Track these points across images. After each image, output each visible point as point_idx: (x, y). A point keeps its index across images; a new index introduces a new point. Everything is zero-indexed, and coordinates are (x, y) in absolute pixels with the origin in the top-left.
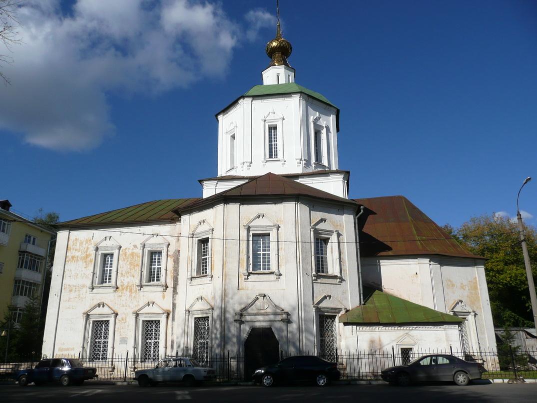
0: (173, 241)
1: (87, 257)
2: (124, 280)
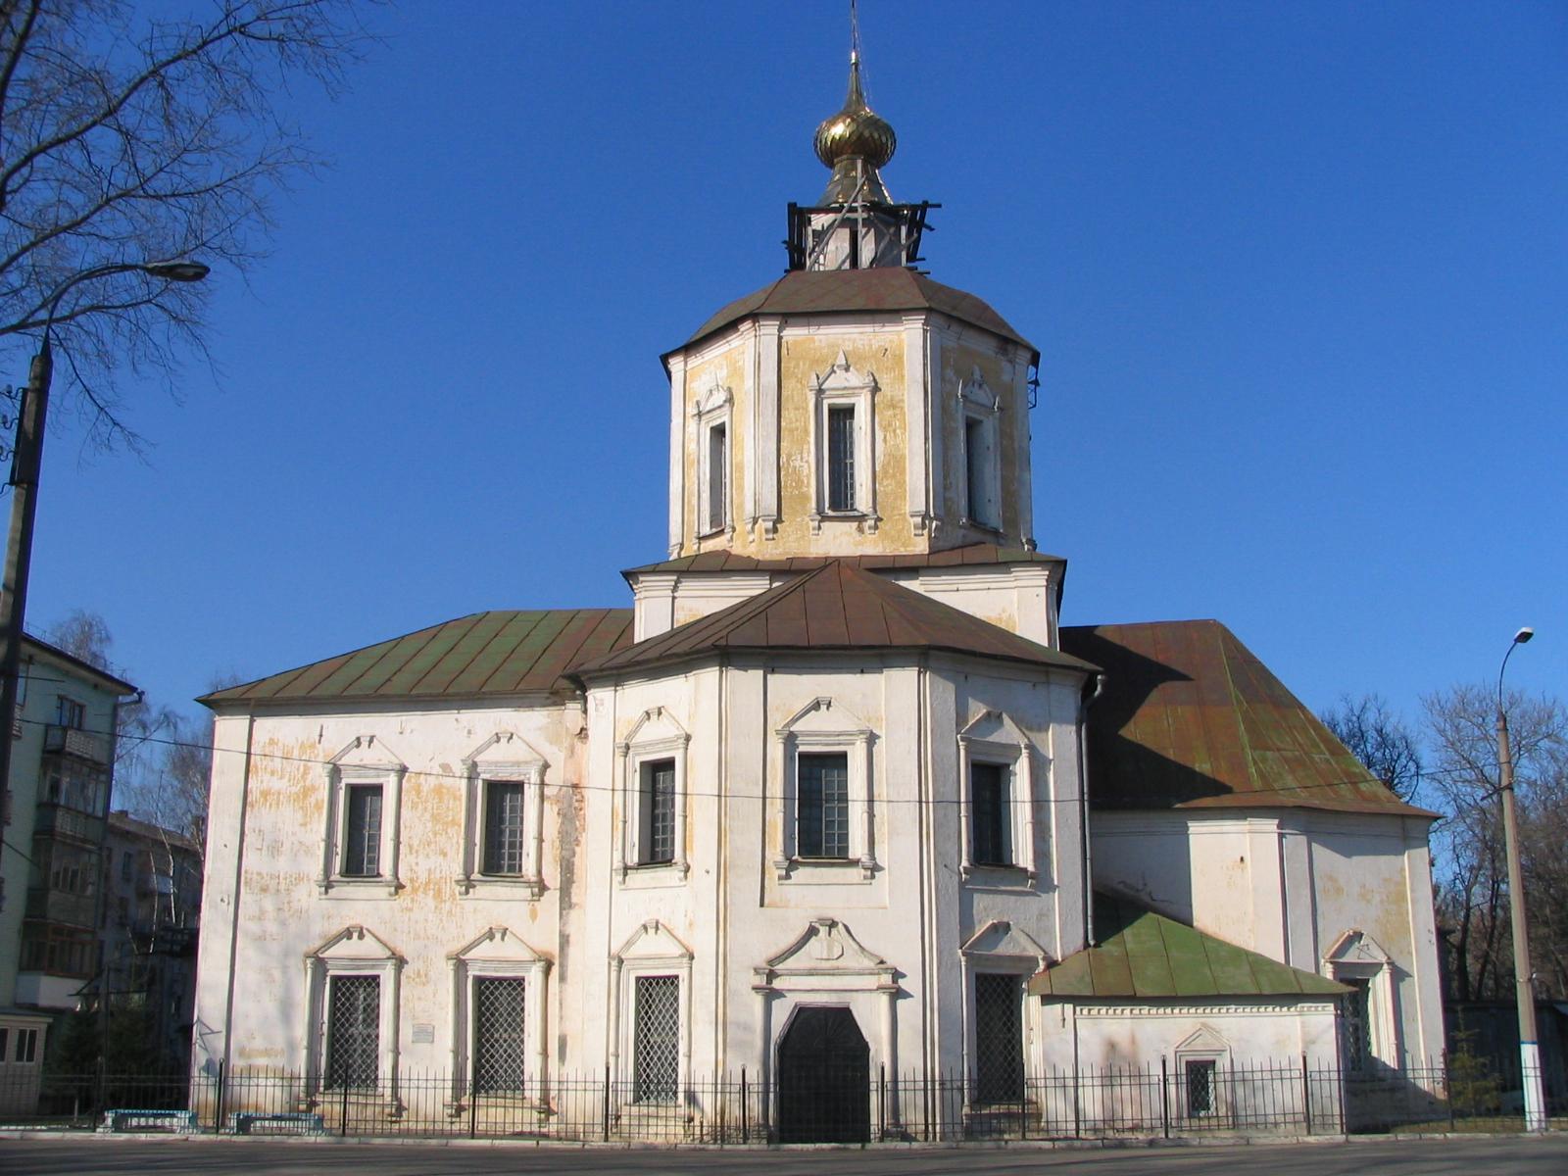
0: (556, 756)
1: (305, 796)
2: (417, 864)
